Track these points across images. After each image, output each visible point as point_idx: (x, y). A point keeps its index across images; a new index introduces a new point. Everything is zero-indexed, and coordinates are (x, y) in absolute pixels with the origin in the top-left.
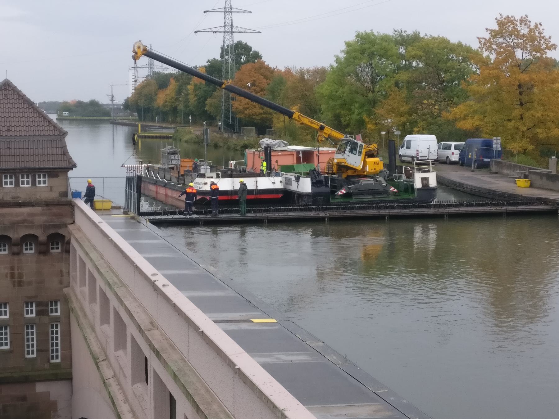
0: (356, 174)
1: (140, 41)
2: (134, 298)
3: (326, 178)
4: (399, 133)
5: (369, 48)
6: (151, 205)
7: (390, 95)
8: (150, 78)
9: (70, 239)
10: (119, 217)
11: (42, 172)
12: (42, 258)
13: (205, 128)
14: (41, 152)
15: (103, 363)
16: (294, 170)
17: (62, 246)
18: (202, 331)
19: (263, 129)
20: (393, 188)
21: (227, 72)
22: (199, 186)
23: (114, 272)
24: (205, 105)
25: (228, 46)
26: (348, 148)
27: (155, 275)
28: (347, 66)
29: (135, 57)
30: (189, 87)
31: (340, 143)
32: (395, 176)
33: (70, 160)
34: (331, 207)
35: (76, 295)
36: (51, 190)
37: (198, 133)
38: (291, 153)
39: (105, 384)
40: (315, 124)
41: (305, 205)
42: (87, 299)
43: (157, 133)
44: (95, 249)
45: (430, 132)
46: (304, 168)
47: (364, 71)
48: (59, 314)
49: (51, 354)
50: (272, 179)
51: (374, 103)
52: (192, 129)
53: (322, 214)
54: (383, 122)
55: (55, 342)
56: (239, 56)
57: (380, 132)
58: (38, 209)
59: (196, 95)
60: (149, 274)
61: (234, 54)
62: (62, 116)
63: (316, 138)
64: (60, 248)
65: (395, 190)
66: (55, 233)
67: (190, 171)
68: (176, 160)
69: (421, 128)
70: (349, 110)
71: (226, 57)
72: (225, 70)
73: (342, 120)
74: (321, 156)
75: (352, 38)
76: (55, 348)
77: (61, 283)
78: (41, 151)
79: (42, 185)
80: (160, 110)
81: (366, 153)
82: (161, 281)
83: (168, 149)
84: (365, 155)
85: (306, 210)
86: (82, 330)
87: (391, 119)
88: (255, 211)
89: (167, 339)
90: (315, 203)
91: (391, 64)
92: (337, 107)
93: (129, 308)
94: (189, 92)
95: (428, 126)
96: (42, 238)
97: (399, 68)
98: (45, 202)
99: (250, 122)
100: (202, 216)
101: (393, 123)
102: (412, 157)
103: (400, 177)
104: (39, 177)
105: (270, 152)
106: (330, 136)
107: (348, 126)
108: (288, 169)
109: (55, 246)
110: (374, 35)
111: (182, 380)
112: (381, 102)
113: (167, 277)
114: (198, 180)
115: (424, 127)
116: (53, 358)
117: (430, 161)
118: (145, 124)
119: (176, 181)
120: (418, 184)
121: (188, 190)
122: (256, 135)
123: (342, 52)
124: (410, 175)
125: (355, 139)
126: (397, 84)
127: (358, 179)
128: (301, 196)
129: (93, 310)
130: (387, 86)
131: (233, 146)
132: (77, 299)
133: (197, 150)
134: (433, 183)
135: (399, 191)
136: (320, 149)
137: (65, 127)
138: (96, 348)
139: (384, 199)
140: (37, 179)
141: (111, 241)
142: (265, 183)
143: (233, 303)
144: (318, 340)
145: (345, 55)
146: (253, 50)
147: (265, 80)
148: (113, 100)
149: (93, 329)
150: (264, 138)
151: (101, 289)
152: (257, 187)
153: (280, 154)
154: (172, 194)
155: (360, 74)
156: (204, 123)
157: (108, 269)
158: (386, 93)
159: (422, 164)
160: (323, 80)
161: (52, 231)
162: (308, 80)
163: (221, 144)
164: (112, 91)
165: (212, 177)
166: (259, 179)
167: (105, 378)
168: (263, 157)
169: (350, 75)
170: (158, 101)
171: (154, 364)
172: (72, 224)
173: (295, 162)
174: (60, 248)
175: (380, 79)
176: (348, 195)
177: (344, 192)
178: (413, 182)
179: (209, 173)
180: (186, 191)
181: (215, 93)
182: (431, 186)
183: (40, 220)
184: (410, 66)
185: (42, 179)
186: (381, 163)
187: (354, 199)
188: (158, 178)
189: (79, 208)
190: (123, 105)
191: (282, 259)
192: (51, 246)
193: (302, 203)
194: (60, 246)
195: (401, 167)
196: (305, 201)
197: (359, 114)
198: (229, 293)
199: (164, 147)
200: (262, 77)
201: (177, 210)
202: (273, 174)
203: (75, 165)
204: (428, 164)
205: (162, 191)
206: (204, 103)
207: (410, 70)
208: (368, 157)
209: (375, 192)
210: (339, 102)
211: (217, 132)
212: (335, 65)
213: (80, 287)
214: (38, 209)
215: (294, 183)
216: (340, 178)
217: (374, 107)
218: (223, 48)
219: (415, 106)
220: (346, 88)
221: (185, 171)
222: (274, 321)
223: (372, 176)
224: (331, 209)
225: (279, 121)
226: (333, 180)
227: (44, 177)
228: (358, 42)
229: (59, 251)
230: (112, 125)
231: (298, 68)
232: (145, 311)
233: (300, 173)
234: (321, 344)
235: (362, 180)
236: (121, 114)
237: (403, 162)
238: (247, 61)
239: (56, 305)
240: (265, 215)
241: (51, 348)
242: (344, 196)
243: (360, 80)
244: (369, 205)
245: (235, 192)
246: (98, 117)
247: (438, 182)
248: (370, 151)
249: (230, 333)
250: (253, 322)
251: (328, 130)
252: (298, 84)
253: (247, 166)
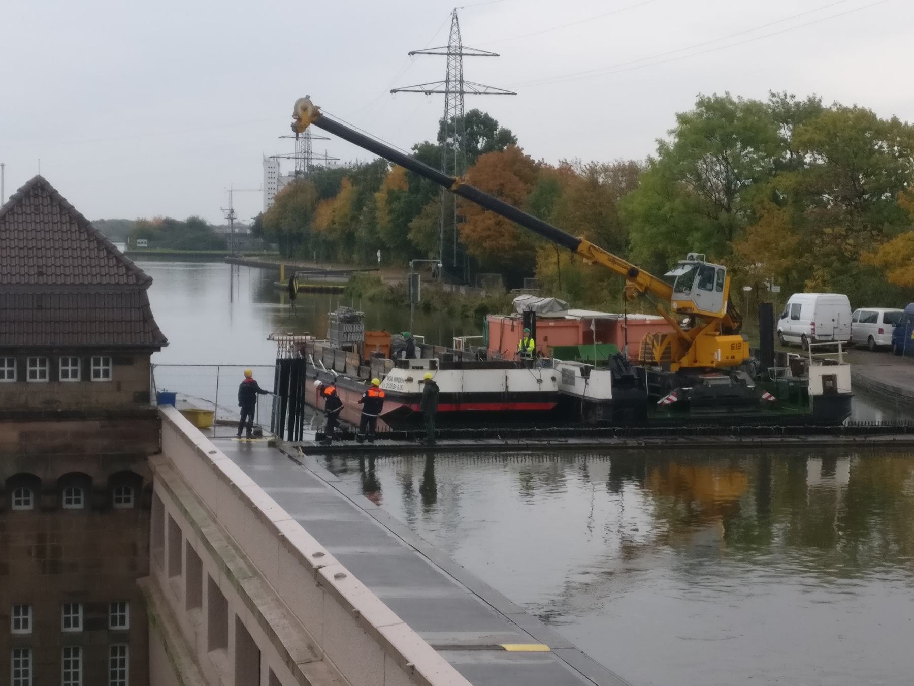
1: (308, 97)
2: (278, 600)
4: (776, 289)
7: (762, 216)
8: (302, 176)
9: (152, 483)
10: (232, 439)
13: (411, 274)
16: (579, 356)
19: (518, 275)
20: (767, 394)
22: (397, 383)
24: (409, 230)
27: (319, 555)
29: (298, 128)
30: (377, 195)
35: (161, 591)
36: (119, 388)
37: (393, 283)
38: (573, 324)
45: (837, 289)
46: (596, 351)
47: (712, 169)
48: (127, 626)
50: (536, 373)
54: (747, 268)
56: (473, 137)
57: (741, 287)
59: (391, 212)
60: (308, 554)
62: (135, 247)
64: (132, 499)
65: (772, 398)
69: (819, 281)
71: (450, 140)
72: (448, 164)
75: (689, 107)
82: (330, 568)
87: (762, 262)
88: (504, 436)
91: (763, 158)
93: (268, 618)
95: (832, 277)
96: (100, 479)
97: (779, 165)
102: (803, 336)
104: (97, 363)
108: (567, 353)
110: (732, 103)
112: (743, 229)
113: (340, 558)
115: (826, 278)
117: (840, 343)
118: (290, 264)
120: (815, 388)
122: (504, 290)
123: (671, 132)
124: (800, 370)
128: (590, 405)
134: (844, 385)
137: (146, 267)
142: (522, 381)
145: (677, 140)
146: (499, 127)
147: (521, 185)
150: (520, 294)
151: (211, 582)
152: (507, 387)
153: (552, 324)
155: (704, 177)
157: (226, 543)
158: (754, 213)
159: (824, 349)
160: (632, 185)
162: (603, 185)
164: (231, 202)
165: (422, 368)
172: (156, 453)
174: (132, 499)
177: (675, 399)
178: (807, 383)
181: (427, 207)
182: (840, 391)
184: (801, 163)
185: (101, 368)
187: (693, 413)
188: (320, 366)
189: (171, 423)
192: (115, 496)
194: (132, 497)
200: (517, 179)
203: (164, 342)
204: (835, 349)
210: (663, 228)
211: (429, 281)
212: (657, 157)
217: (730, 240)
218: (443, 123)
224: (649, 434)
226: (653, 376)
227: (106, 363)
228: (700, 115)
237: (785, 344)
238: (488, 148)
242: (673, 406)
243: (703, 188)
247: (854, 384)
253: (488, 347)
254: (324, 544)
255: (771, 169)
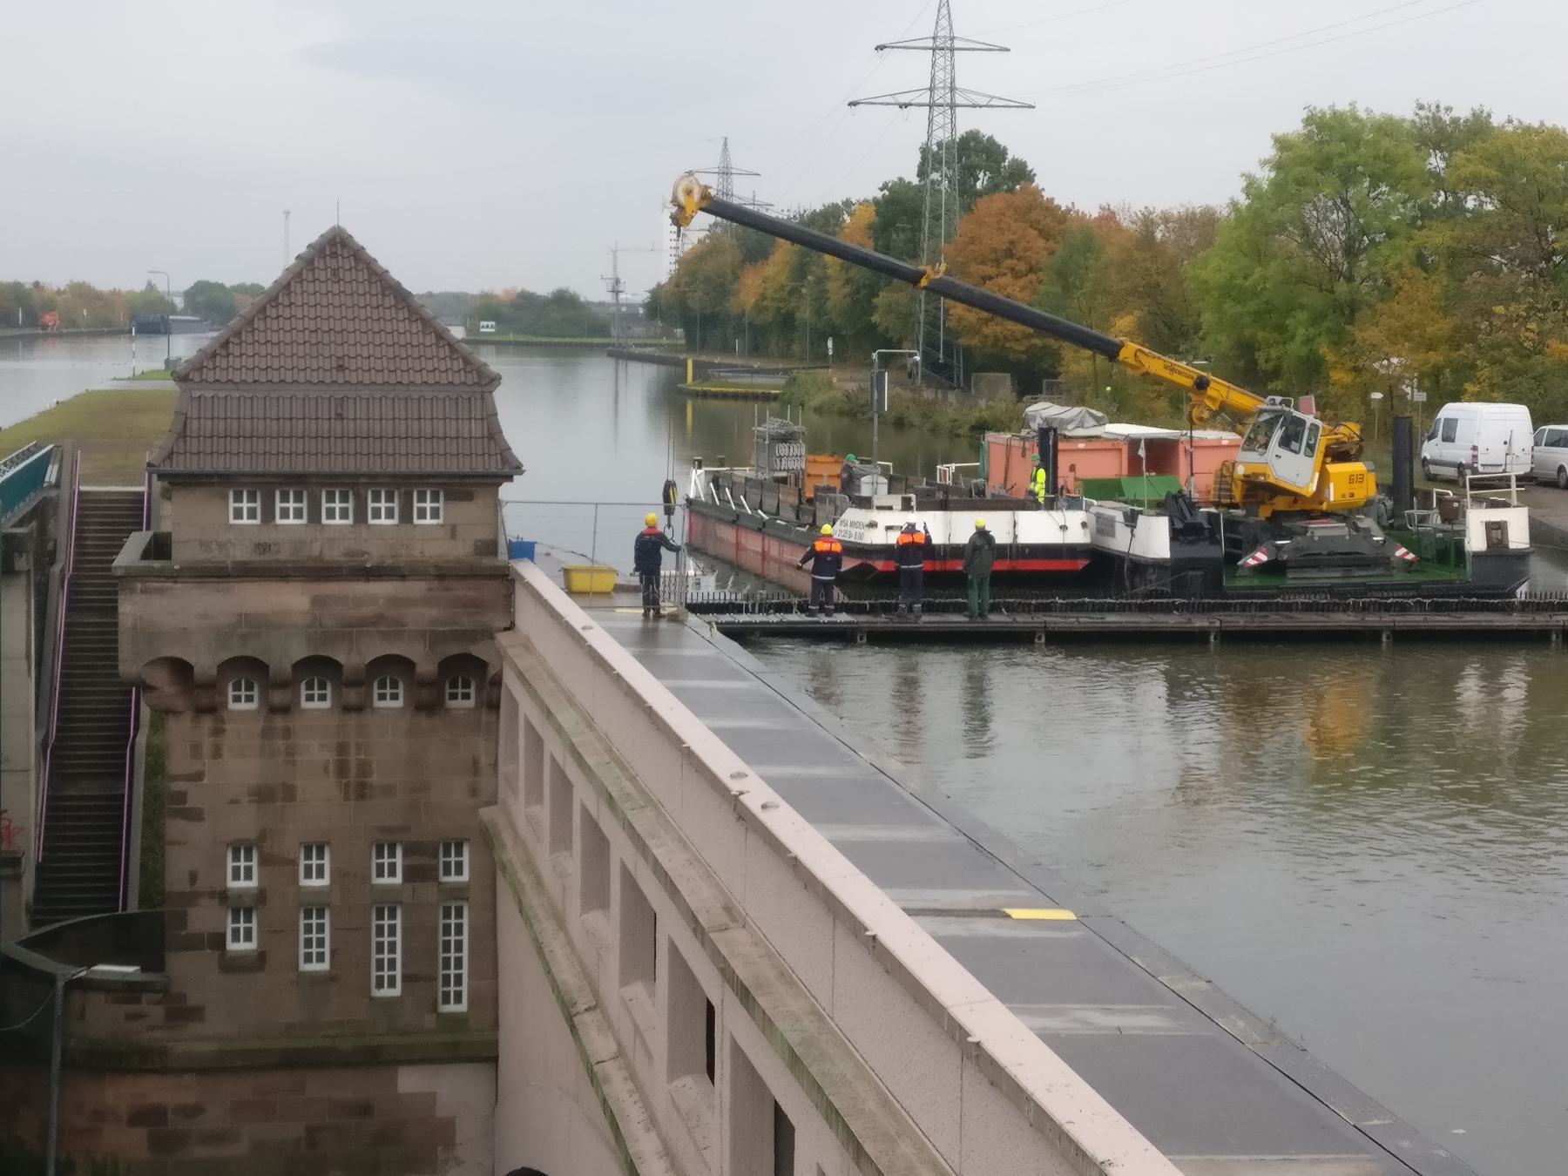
0: (1297, 507)
2: (681, 840)
3: (1212, 518)
4: (1421, 397)
5: (1341, 155)
6: (721, 583)
8: (719, 230)
11: (430, 485)
12: (424, 721)
14: (429, 430)
15: (587, 1017)
17: (479, 690)
18: (874, 937)
19: (1033, 379)
20: (1404, 550)
21: (937, 218)
22: (854, 531)
23: (623, 768)
25: (939, 145)
26: (1278, 434)
28: (1279, 205)
31: (1251, 421)
32: (1411, 517)
33: (505, 453)
34: (1223, 609)
36: (453, 536)
37: (851, 386)
38: (1113, 444)
39: (592, 1076)
40: (1182, 371)
41: (1150, 595)
42: (547, 840)
43: (732, 385)
44: (570, 700)
46: (1149, 486)
47: (1326, 219)
48: (465, 877)
49: (441, 989)
50: (1058, 516)
51: (1353, 311)
52: (834, 376)
53: (1200, 622)
54: (1376, 365)
55: (452, 955)
56: (970, 172)
57: (1367, 393)
58: (416, 588)
59: (848, 281)
60: (723, 774)
61: (957, 166)
62: (478, 333)
63: (1186, 408)
65: (1411, 556)
66: (459, 656)
67: (830, 489)
68: (793, 458)
70: (1280, 328)
71: (935, 176)
72: (932, 211)
73: (1261, 356)
74: (1197, 454)
75: (1293, 126)
76: (452, 972)
77: (474, 792)
78: (427, 428)
79: (428, 521)
80: (746, 320)
81: (1327, 447)
82: (755, 792)
83: (772, 425)
84: (1326, 456)
85: (1153, 609)
86: (528, 922)
87: (1399, 356)
88: (1011, 609)
89: (770, 955)
90: (1179, 587)
91: (1404, 203)
92: (1246, 320)
93: (666, 866)
94: (830, 271)
96: (426, 666)
97: (1426, 213)
98: (437, 567)
99: (998, 361)
100: (863, 618)
101: (1406, 368)
102: (1460, 466)
103: (1423, 519)
104: (422, 499)
105: (1055, 444)
106: (1224, 407)
107: (1276, 374)
108: (1104, 489)
109: (460, 691)
110: (1356, 119)
111: (813, 1070)
112: (1371, 307)
113: (772, 782)
114: (852, 514)
116: (446, 1000)
118: (704, 358)
119: (791, 515)
121: (821, 546)
122: (1013, 397)
123: (1264, 163)
124: (1453, 515)
125: (1296, 408)
126: (1420, 260)
127: (1303, 523)
128: (1141, 567)
129: (562, 871)
130: (1391, 263)
131: (948, 424)
132: (517, 838)
133: (848, 432)
135: (1422, 560)
136: (1197, 434)
137: (493, 362)
138: (568, 975)
139: (1376, 581)
140: (416, 505)
141: (618, 678)
142: (1039, 528)
143: (955, 862)
144: (1195, 975)
145: (1273, 175)
146: (1010, 157)
147: (1041, 243)
148: (616, 292)
149: (561, 925)
151: (585, 812)
152: (1015, 537)
153: (1081, 446)
154: (781, 552)
155: (1313, 229)
156: (875, 356)
157: (607, 758)
158: (1388, 283)
160: (1206, 241)
161: (454, 649)
162: (1163, 242)
163: (916, 420)
165: (890, 508)
166: (1024, 516)
167: (593, 1060)
168: (1036, 454)
169: (1285, 229)
170: (742, 296)
171: (733, 1023)
172: (506, 629)
173: (1125, 471)
175: (1372, 241)
176: (1273, 568)
177: (1264, 558)
178: (1462, 533)
179: (883, 497)
180: (813, 547)
183: (423, 616)
184: (1459, 206)
185: (428, 505)
186: (1371, 480)
187: (1292, 579)
190: (645, 306)
191: (1087, 748)
192: (448, 691)
193: (1141, 589)
194: (472, 691)
195: (1428, 495)
196: (1153, 582)
197: (1309, 341)
198: (941, 833)
199: (762, 422)
200: (1035, 233)
201: (795, 601)
202: (1061, 502)
203: (518, 469)
205: (753, 543)
206: (870, 302)
207: (1459, 219)
208: (1333, 461)
209: (1351, 561)
210: (1252, 306)
212: (1243, 201)
213: (528, 804)
214: (416, 588)
215: (1122, 532)
216: (1252, 520)
217: (1351, 323)
218: (925, 151)
219: (1469, 322)
220: (1274, 266)
221: (817, 489)
222: (1067, 915)
223: (1344, 514)
225: (1077, 362)
226: (1232, 524)
227: (435, 499)
228: (1309, 136)
229: (471, 703)
230: (612, 361)
231: (1138, 207)
232: (709, 875)
233: (1140, 503)
234: (1203, 985)
235: (1313, 525)
236: (638, 330)
237: (1432, 478)
238: (993, 188)
239: (459, 853)
240: (1040, 619)
241: (441, 972)
242: (1262, 569)
244: (1338, 598)
245: (954, 551)
246: (574, 336)
248: (1339, 442)
249: (952, 946)
250: (1009, 916)
251: (1220, 389)
252: (1137, 254)
254: (747, 763)
255: (1414, 219)
